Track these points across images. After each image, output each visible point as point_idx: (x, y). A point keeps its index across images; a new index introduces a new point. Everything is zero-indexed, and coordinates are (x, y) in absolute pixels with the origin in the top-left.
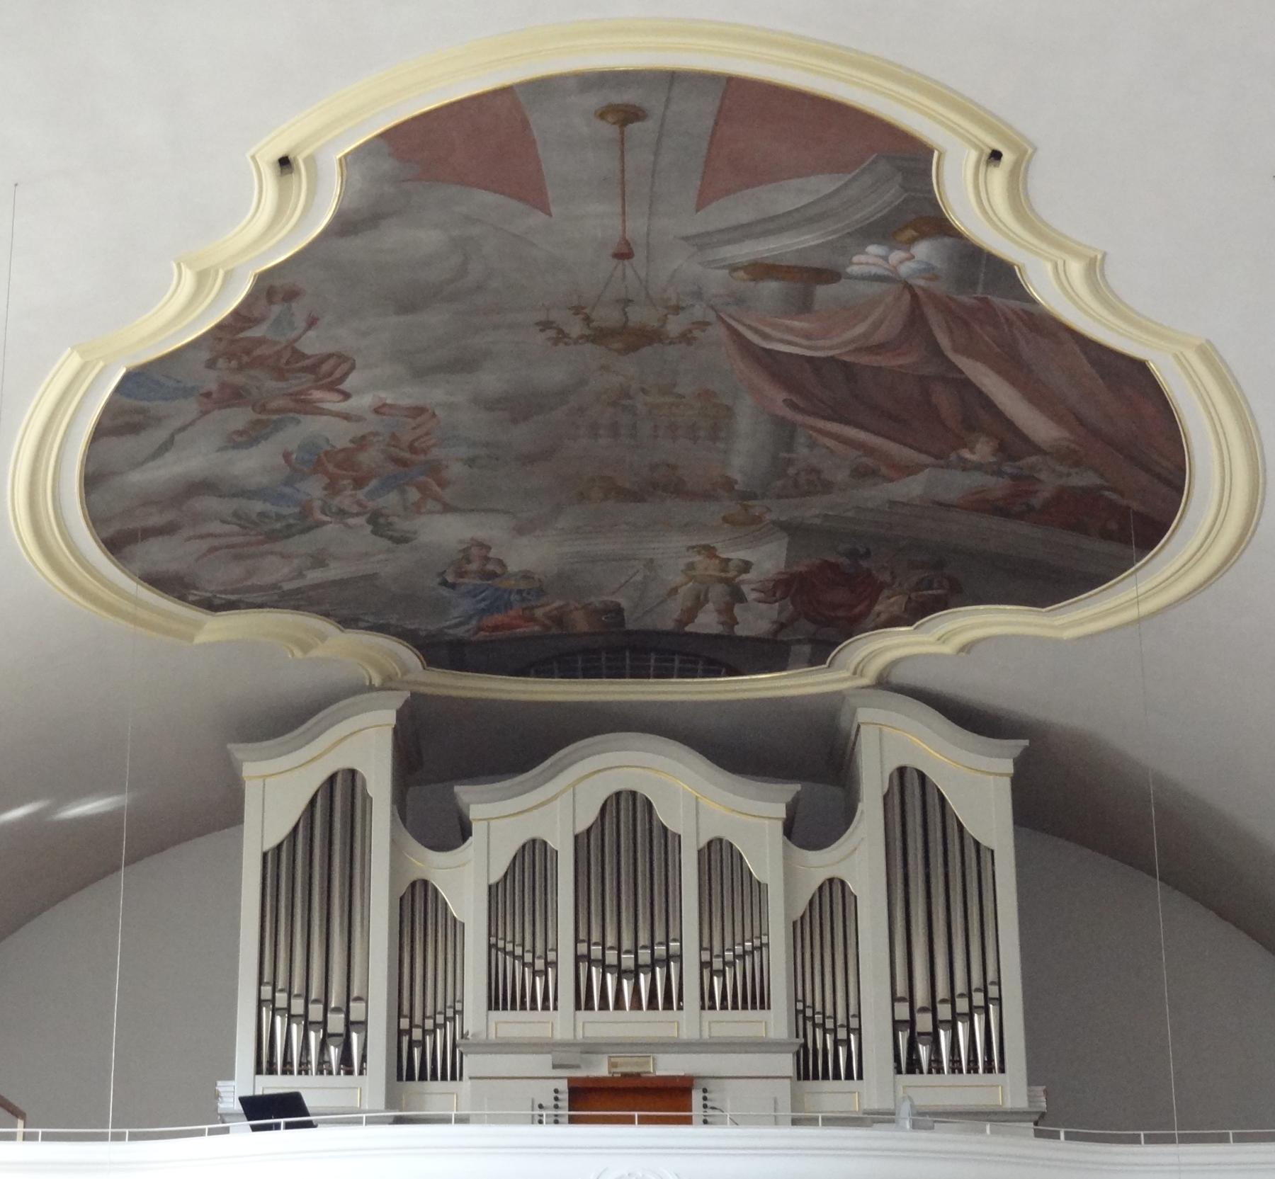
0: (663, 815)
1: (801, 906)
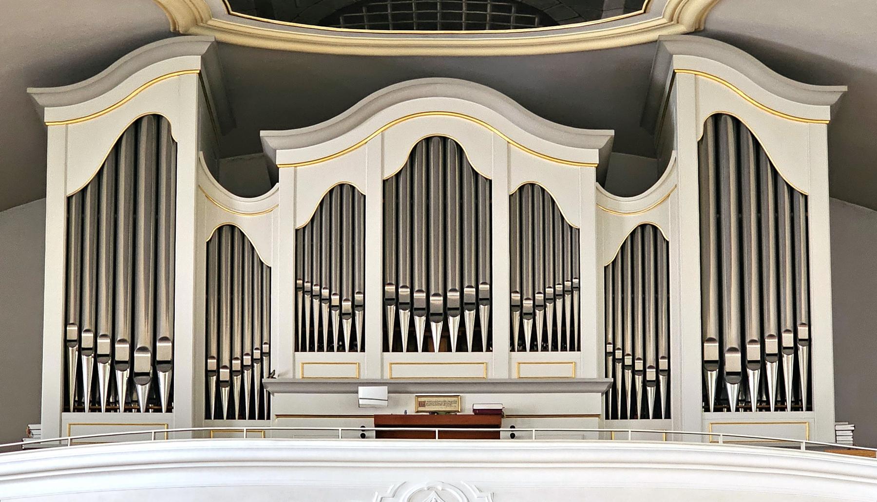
0: (476, 160)
1: (613, 252)
